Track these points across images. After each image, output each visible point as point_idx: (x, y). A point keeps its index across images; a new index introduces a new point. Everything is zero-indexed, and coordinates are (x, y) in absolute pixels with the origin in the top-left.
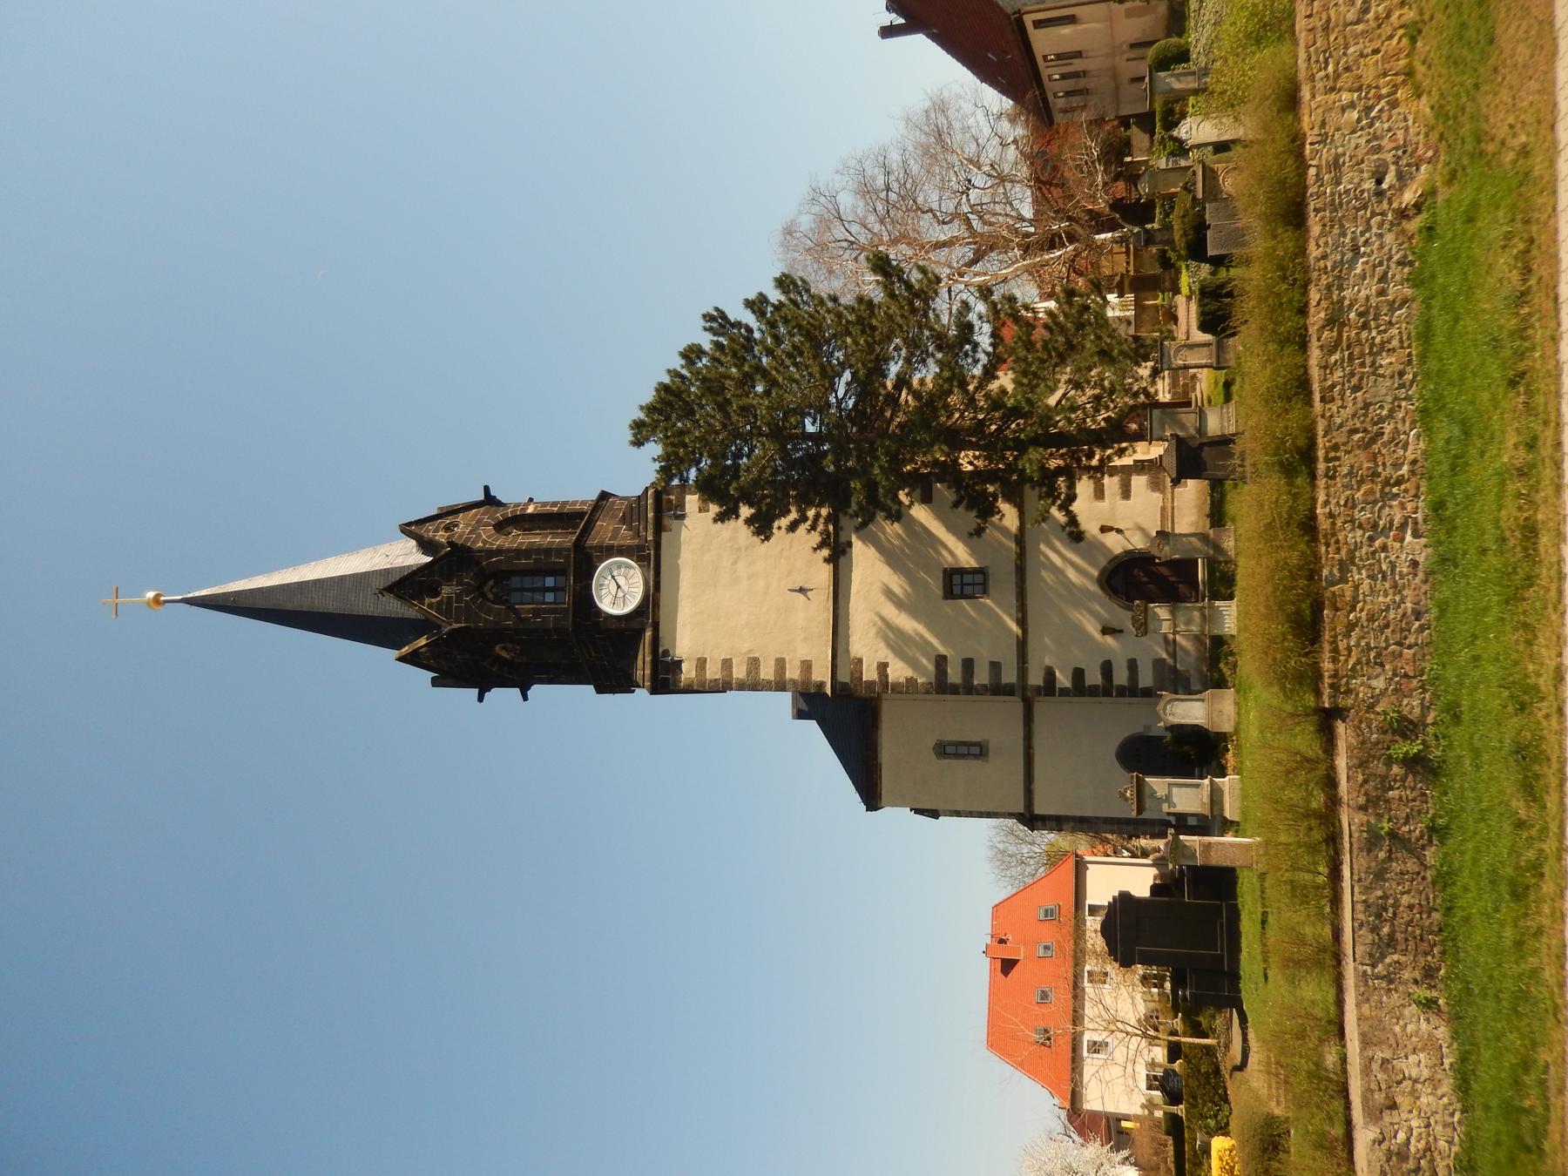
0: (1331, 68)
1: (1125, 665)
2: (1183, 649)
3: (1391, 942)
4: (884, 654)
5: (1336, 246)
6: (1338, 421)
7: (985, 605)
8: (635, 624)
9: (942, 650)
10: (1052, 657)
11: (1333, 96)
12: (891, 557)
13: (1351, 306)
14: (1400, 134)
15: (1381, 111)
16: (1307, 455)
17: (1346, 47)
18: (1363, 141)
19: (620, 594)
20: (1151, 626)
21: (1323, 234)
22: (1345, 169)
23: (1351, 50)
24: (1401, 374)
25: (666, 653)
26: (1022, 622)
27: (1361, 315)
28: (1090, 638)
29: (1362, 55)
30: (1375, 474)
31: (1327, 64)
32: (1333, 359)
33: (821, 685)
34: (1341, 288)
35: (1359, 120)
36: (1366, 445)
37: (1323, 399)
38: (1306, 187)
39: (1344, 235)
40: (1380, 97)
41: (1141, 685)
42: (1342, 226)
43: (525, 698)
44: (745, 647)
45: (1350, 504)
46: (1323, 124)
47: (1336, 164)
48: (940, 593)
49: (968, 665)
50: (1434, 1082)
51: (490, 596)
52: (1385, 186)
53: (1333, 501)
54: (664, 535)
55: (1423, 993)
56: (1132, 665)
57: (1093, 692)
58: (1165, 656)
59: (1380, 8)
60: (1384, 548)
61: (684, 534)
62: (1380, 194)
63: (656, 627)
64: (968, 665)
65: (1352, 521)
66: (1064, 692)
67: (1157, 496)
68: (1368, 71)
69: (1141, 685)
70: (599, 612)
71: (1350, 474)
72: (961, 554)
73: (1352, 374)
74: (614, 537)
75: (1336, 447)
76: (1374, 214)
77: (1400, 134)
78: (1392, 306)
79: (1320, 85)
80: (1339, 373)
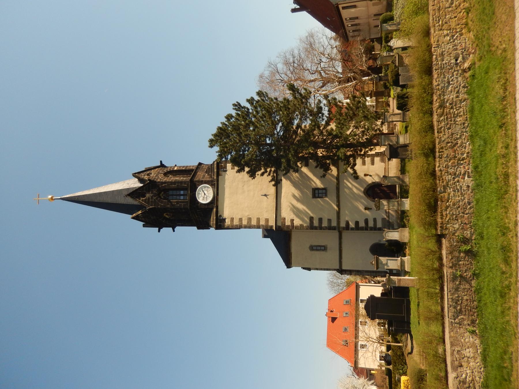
0: (440, 23)
1: (372, 220)
2: (392, 215)
3: (460, 312)
4: (293, 216)
5: (442, 81)
6: (443, 139)
7: (326, 200)
8: (210, 207)
9: (312, 215)
10: (348, 217)
11: (441, 32)
12: (295, 184)
13: (447, 101)
14: (463, 44)
15: (457, 37)
16: (433, 151)
17: (446, 15)
18: (451, 47)
19: (205, 197)
20: (381, 207)
21: (438, 77)
22: (445, 56)
23: (447, 17)
24: (464, 124)
25: (221, 216)
26: (338, 206)
27: (450, 104)
28: (361, 211)
29: (451, 18)
30: (455, 157)
31: (439, 21)
32: (441, 119)
33: (272, 226)
34: (444, 95)
35: (450, 40)
36: (452, 147)
37: (438, 132)
38: (432, 62)
39: (445, 78)
40: (457, 32)
41: (378, 227)
42: (444, 75)
43: (174, 231)
44: (247, 214)
45: (447, 167)
46: (438, 41)
47: (442, 54)
48: (311, 196)
49: (320, 220)
50: (474, 358)
51: (162, 197)
52: (458, 61)
53: (441, 166)
54: (220, 177)
55: (471, 328)
56: (375, 220)
57: (362, 229)
58: (385, 217)
59: (457, 3)
60: (458, 181)
61: (227, 177)
62: (457, 64)
63: (217, 207)
64: (320, 220)
65: (448, 172)
66: (352, 229)
67: (383, 164)
68: (453, 23)
69: (378, 227)
70: (198, 202)
71: (447, 157)
72: (318, 183)
73: (448, 124)
74: (203, 178)
75: (442, 148)
76: (455, 71)
77: (463, 44)
78: (461, 101)
79: (437, 28)
80: (443, 124)
